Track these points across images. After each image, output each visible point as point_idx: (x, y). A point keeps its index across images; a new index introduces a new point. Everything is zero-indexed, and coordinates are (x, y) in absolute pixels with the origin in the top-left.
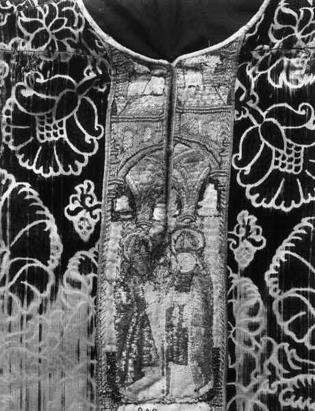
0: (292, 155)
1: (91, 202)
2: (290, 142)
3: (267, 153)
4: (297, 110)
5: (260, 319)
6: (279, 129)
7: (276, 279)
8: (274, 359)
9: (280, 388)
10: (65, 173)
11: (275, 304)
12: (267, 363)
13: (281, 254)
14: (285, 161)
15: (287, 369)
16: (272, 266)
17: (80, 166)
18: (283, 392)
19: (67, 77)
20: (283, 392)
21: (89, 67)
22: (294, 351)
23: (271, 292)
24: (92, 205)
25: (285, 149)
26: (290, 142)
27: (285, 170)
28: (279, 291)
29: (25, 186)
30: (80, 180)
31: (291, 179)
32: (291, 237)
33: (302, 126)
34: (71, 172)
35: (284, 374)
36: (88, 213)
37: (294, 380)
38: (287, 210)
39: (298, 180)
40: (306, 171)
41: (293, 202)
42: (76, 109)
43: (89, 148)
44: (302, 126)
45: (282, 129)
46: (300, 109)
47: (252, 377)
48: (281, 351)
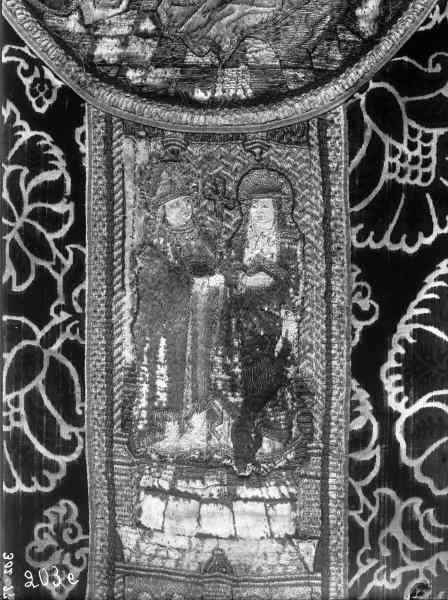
0: (418, 152)
1: (73, 536)
2: (415, 125)
3: (376, 148)
4: (426, 65)
5: (372, 453)
6: (396, 100)
7: (399, 377)
8: (395, 529)
9: (408, 577)
10: (26, 489)
11: (399, 425)
12: (383, 535)
13: (405, 330)
14: (405, 165)
15: (418, 544)
16: (392, 354)
17: (54, 479)
18: (412, 584)
19: (23, 319)
20: (412, 584)
21: (60, 301)
22: (430, 511)
23: (392, 402)
24: (76, 541)
25: (405, 141)
26: (415, 125)
27: (405, 180)
28: (405, 399)
29: (45, 139)
30: (52, 499)
31: (416, 194)
32: (422, 295)
33: (437, 93)
34: (36, 487)
35: (412, 552)
36: (68, 555)
37: (430, 565)
38: (411, 250)
39: (428, 196)
40: (441, 179)
41: (421, 234)
42: (42, 375)
43: (67, 447)
44: (437, 93)
45: (402, 101)
46: (430, 65)
47: (359, 564)
48: (408, 512)
